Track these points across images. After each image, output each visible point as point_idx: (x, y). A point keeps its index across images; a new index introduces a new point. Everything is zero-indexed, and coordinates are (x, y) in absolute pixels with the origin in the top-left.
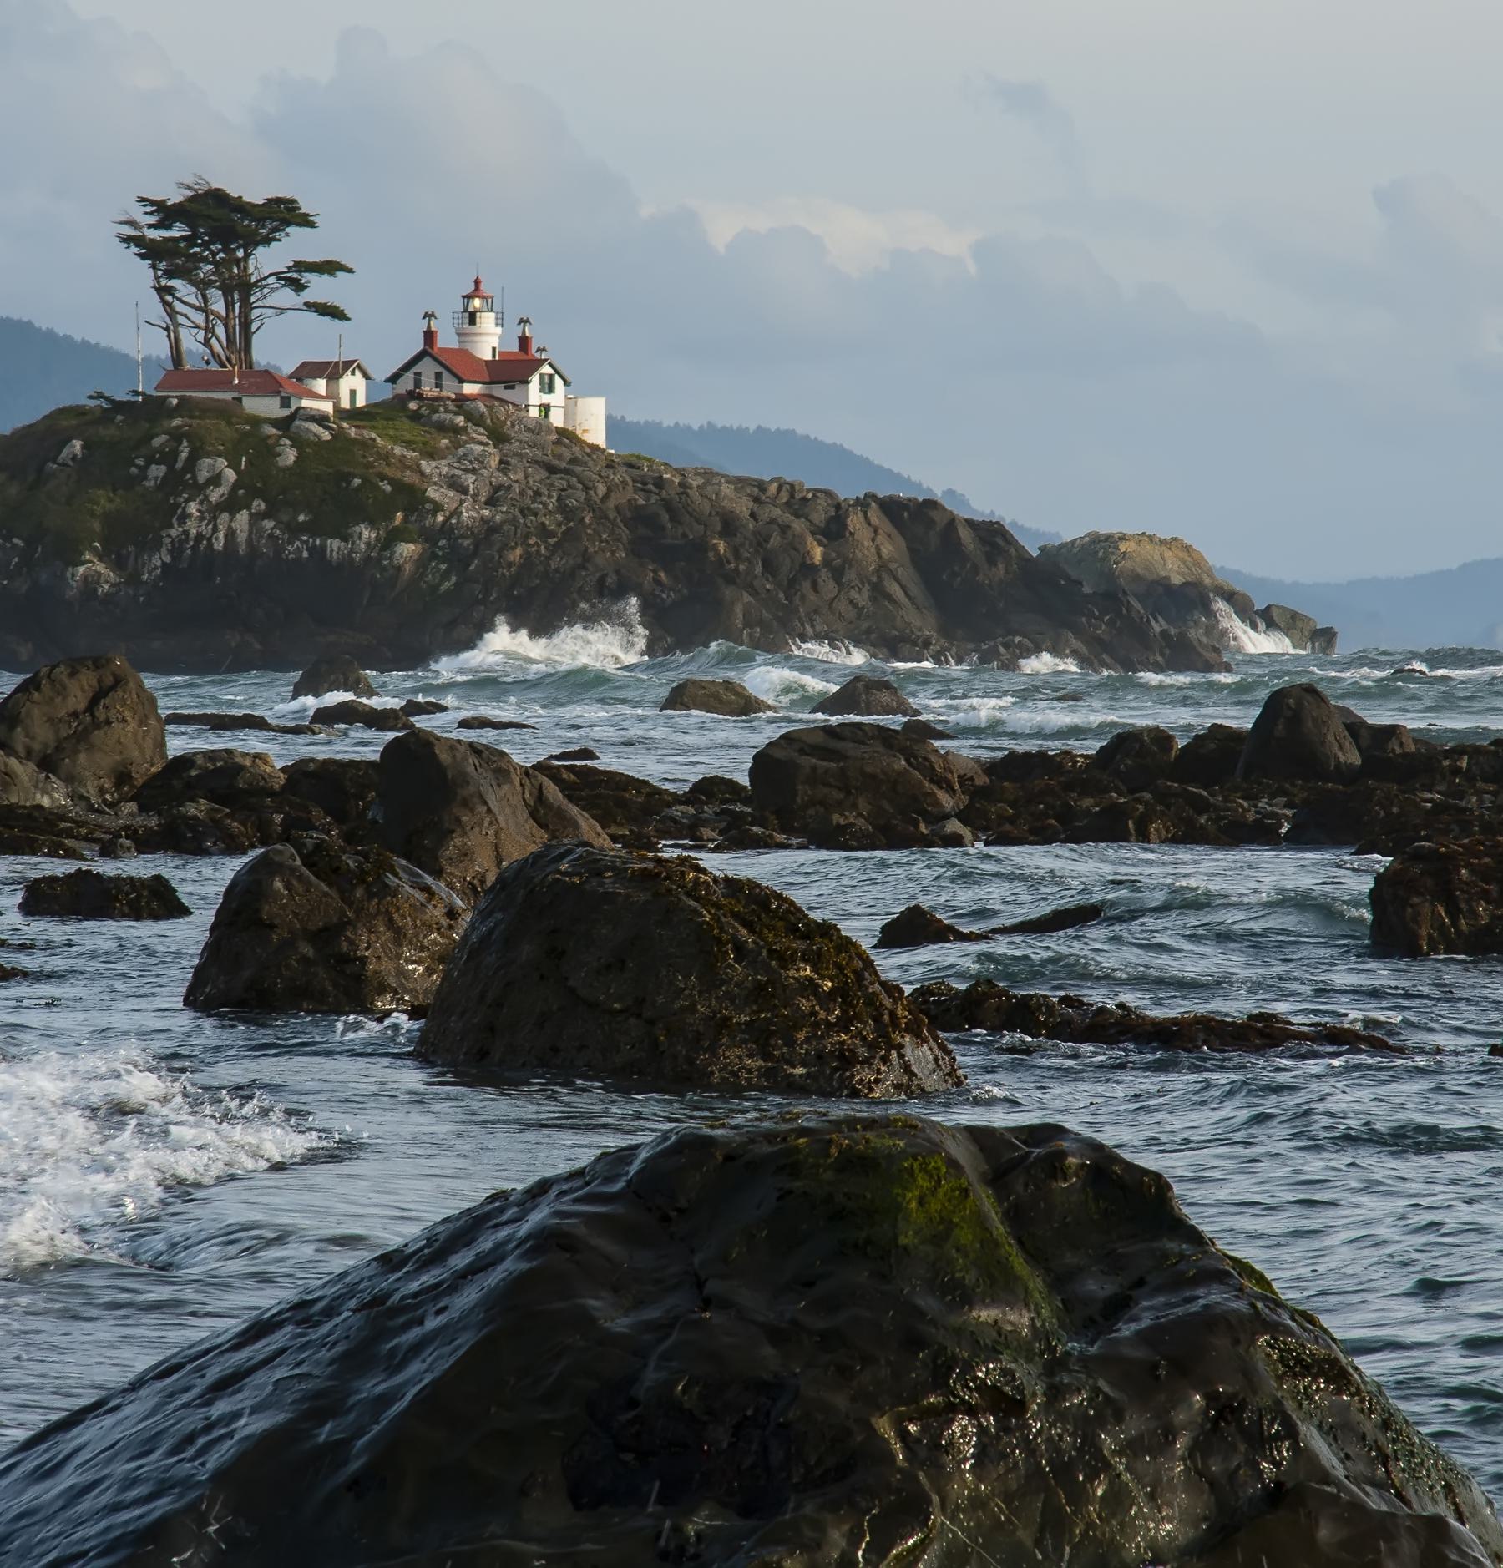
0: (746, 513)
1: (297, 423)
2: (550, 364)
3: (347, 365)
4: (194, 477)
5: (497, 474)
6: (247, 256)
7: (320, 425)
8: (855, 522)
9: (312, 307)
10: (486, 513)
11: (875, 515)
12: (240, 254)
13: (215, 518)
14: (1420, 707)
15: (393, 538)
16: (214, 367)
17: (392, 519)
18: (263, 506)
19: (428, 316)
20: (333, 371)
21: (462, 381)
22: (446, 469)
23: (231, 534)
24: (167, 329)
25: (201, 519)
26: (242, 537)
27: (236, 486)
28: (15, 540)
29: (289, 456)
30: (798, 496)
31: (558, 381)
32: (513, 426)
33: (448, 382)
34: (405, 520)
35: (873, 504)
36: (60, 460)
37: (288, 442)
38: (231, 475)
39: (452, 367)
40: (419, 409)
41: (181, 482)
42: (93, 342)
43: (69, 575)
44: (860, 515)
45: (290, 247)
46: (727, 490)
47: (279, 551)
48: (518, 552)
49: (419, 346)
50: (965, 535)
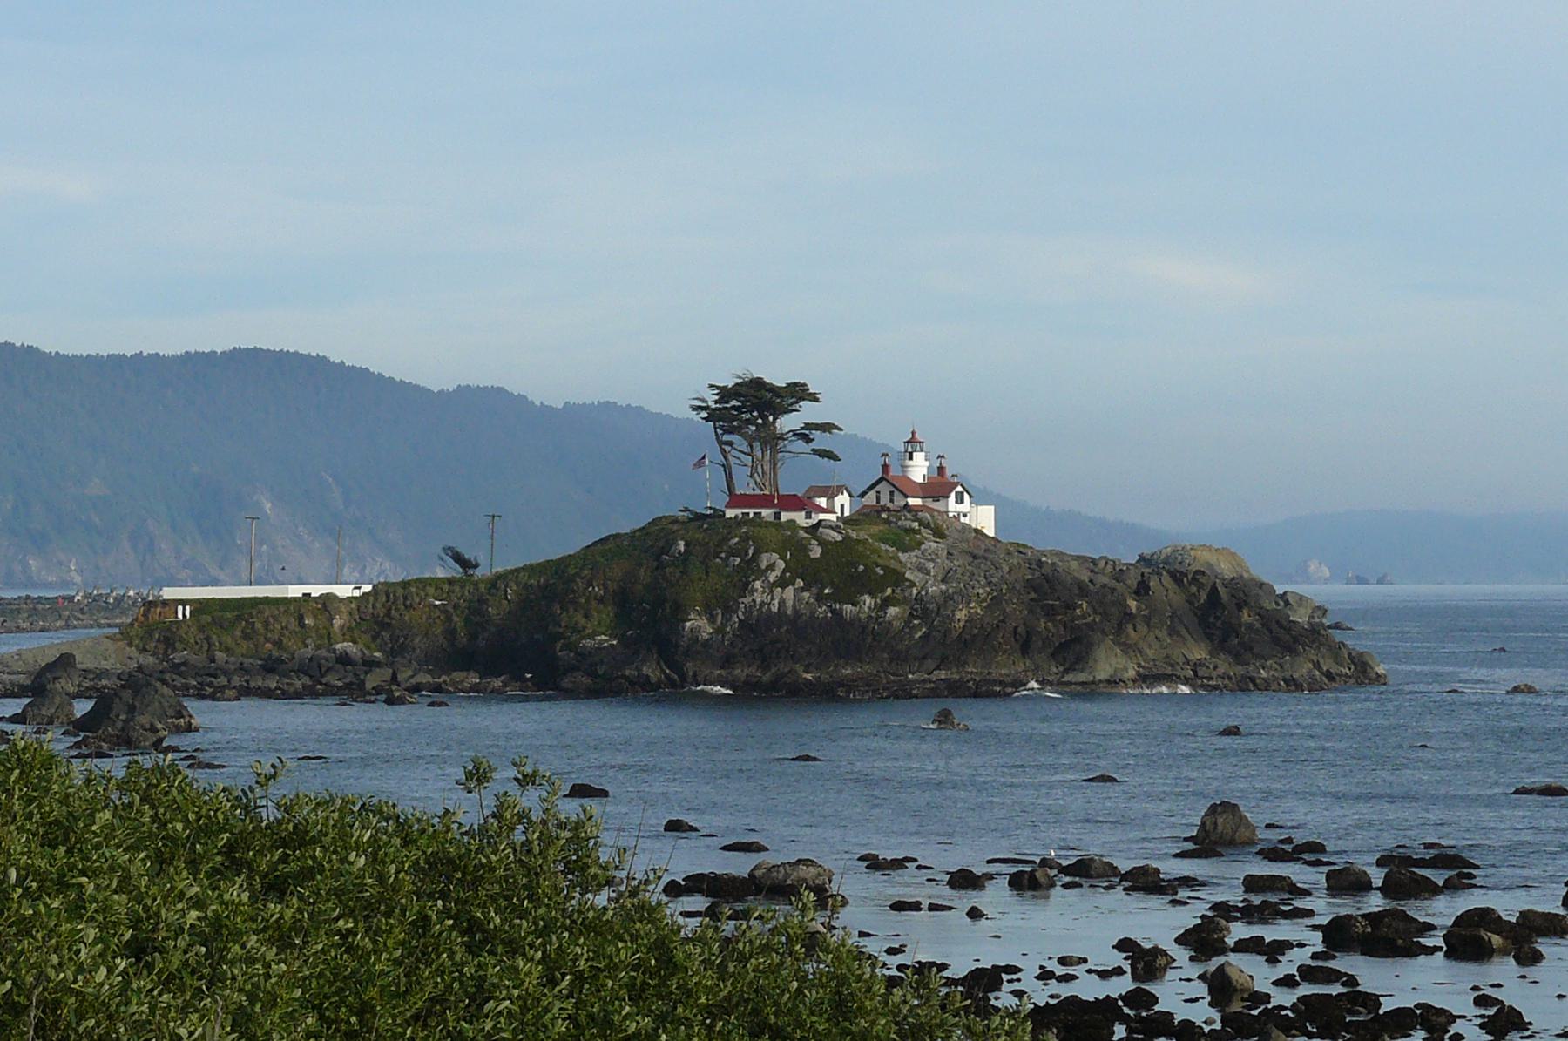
0: (1087, 580)
1: (821, 529)
2: (962, 486)
4: (758, 566)
5: (946, 561)
6: (775, 419)
9: (815, 451)
10: (944, 587)
12: (771, 418)
13: (772, 592)
15: (887, 602)
16: (758, 492)
18: (802, 584)
21: (907, 497)
22: (915, 559)
23: (782, 602)
24: (723, 466)
25: (764, 592)
26: (789, 604)
27: (784, 571)
29: (816, 552)
30: (1117, 569)
31: (966, 496)
33: (897, 496)
35: (1164, 573)
39: (901, 488)
41: (750, 569)
43: (680, 628)
45: (806, 413)
46: (1074, 565)
47: (813, 613)
48: (964, 612)
50: (1221, 590)
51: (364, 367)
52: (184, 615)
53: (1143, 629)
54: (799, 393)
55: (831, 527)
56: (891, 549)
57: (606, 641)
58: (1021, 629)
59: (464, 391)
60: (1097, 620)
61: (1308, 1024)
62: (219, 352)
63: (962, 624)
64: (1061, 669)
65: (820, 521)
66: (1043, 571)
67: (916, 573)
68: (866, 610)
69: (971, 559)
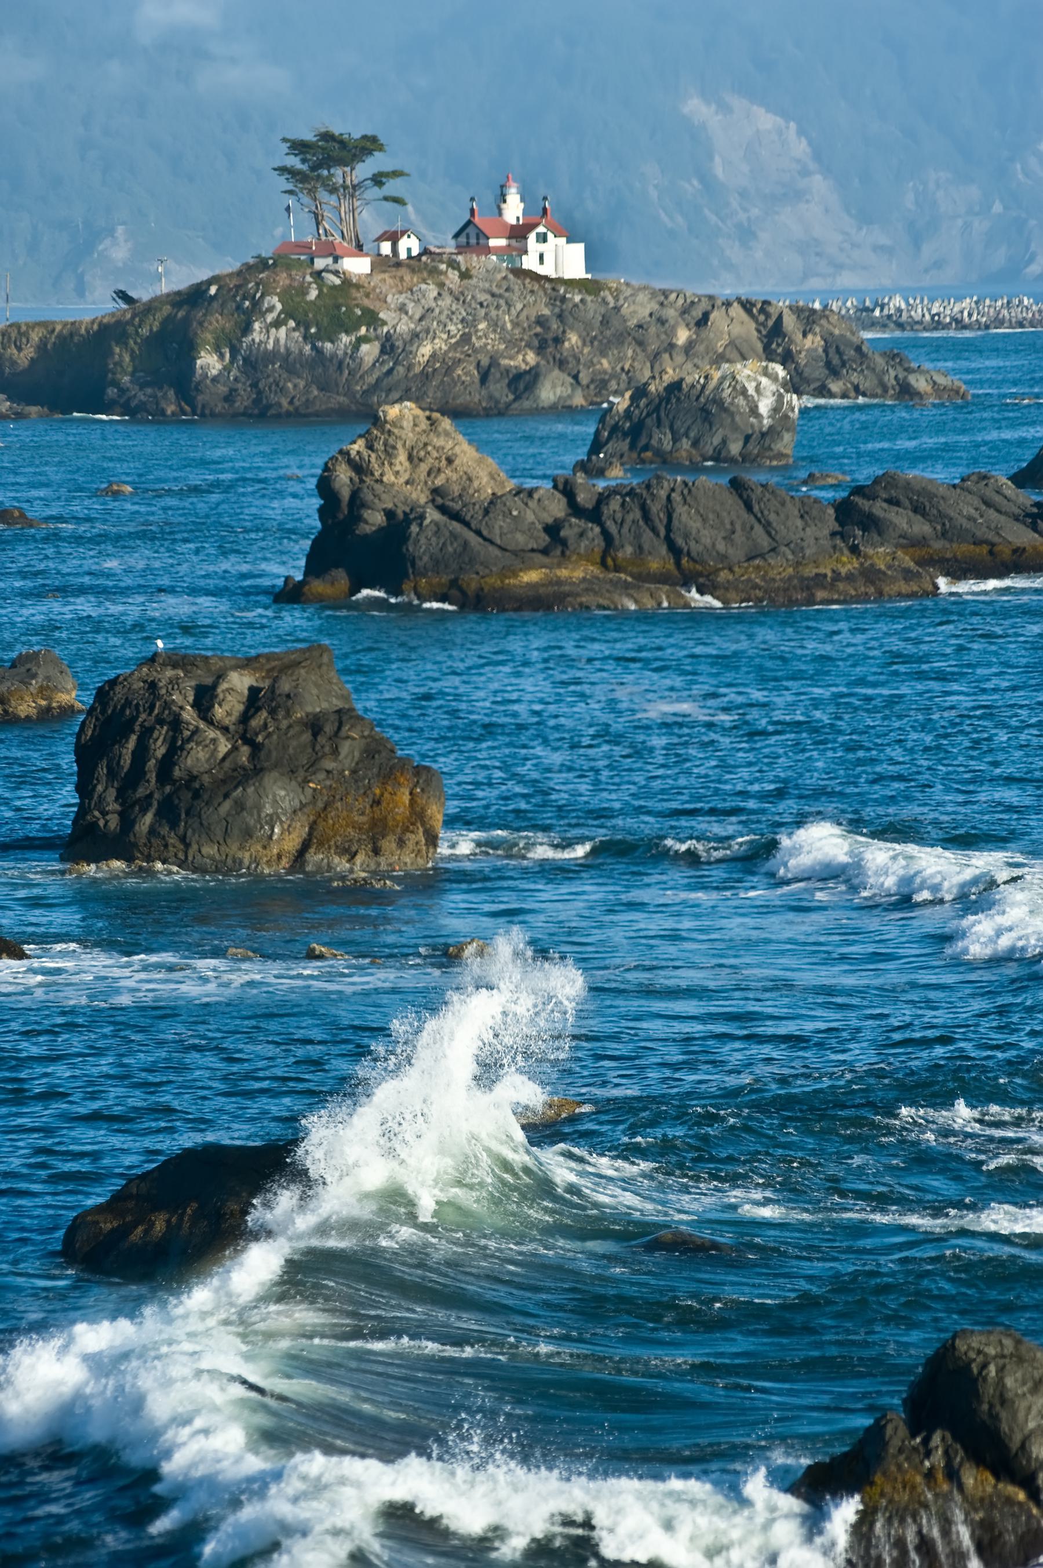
11: (736, 310)
14: (487, 908)
23: (277, 341)
26: (282, 342)
49: (467, 216)
63: (426, 358)
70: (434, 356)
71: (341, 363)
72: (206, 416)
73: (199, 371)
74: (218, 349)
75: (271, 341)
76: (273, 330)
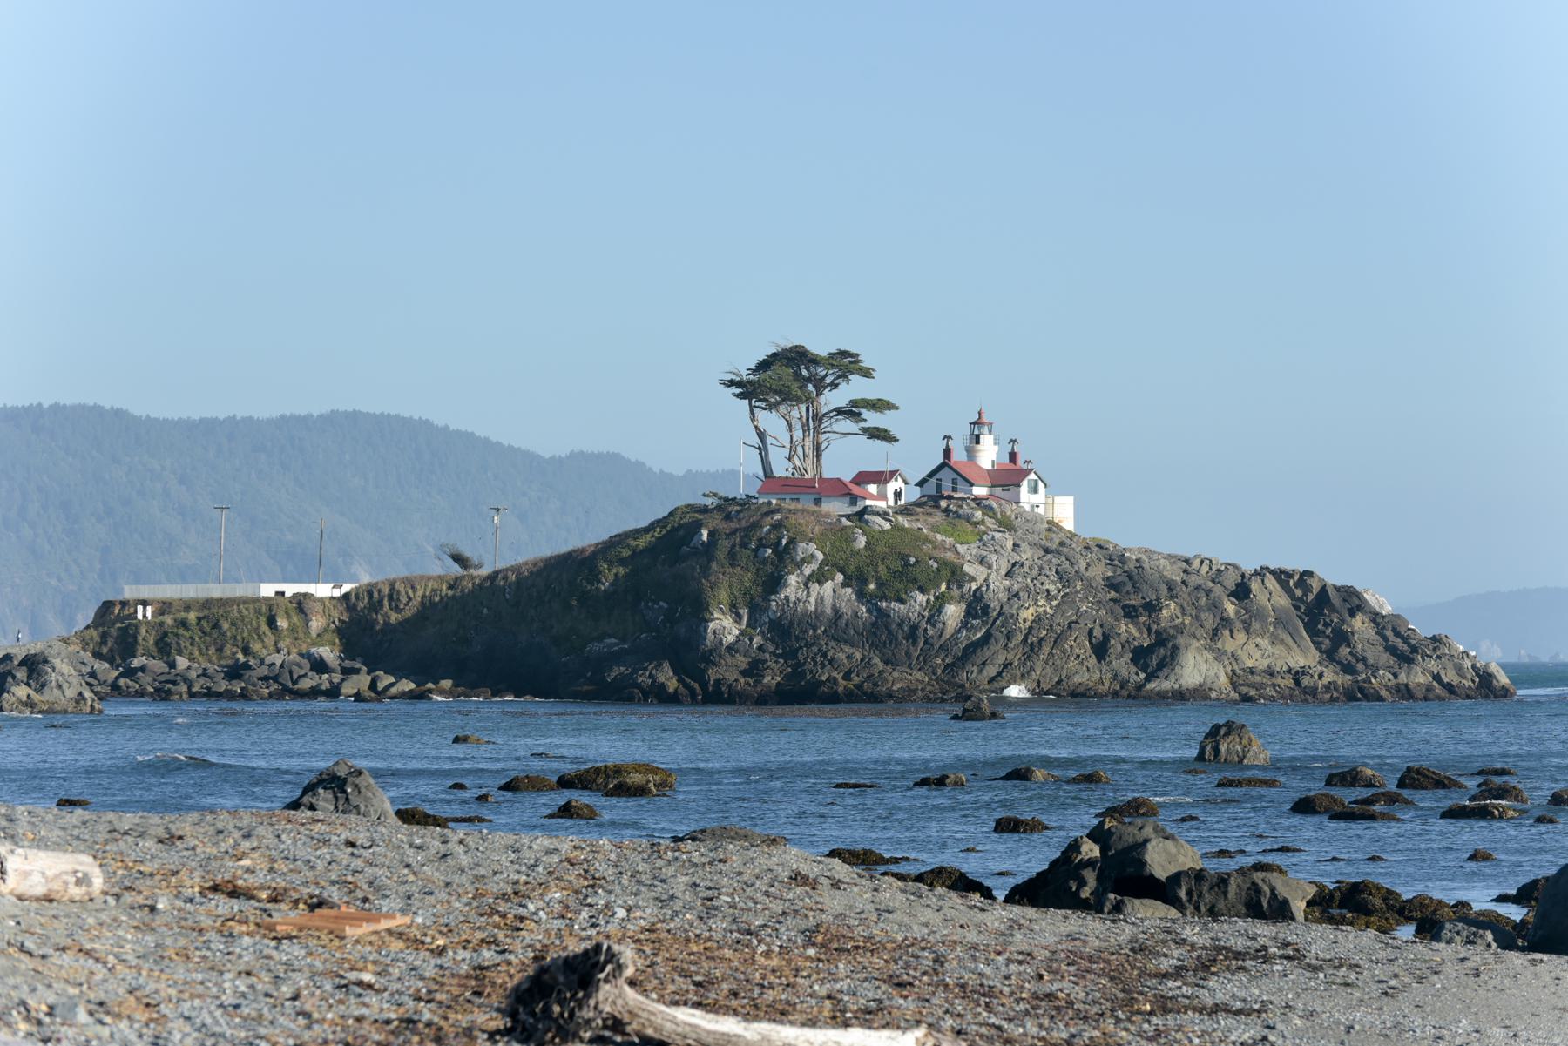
3: (892, 474)
5: (1012, 554)
7: (884, 519)
8: (1255, 586)
10: (1007, 583)
11: (1271, 582)
17: (939, 587)
19: (947, 438)
20: (881, 478)
23: (821, 600)
24: (759, 448)
26: (828, 601)
28: (661, 603)
29: (861, 541)
30: (1214, 568)
31: (1041, 485)
32: (1017, 518)
34: (948, 587)
36: (692, 545)
37: (860, 531)
38: (820, 556)
40: (948, 506)
42: (516, 446)
43: (702, 629)
44: (1260, 581)
48: (1031, 610)
49: (940, 459)
50: (1331, 592)
51: (470, 431)
52: (144, 616)
53: (1241, 637)
54: (846, 364)
55: (878, 514)
56: (948, 540)
57: (616, 645)
58: (1098, 632)
59: (578, 457)
60: (1187, 622)
61: (1110, 854)
62: (316, 415)
63: (1028, 624)
64: (1143, 676)
65: (866, 507)
66: (1126, 568)
67: (977, 566)
68: (917, 607)
69: (1043, 553)
70: (1038, 620)
71: (914, 628)
72: (718, 696)
73: (710, 636)
74: (733, 608)
75: (812, 600)
76: (815, 587)
